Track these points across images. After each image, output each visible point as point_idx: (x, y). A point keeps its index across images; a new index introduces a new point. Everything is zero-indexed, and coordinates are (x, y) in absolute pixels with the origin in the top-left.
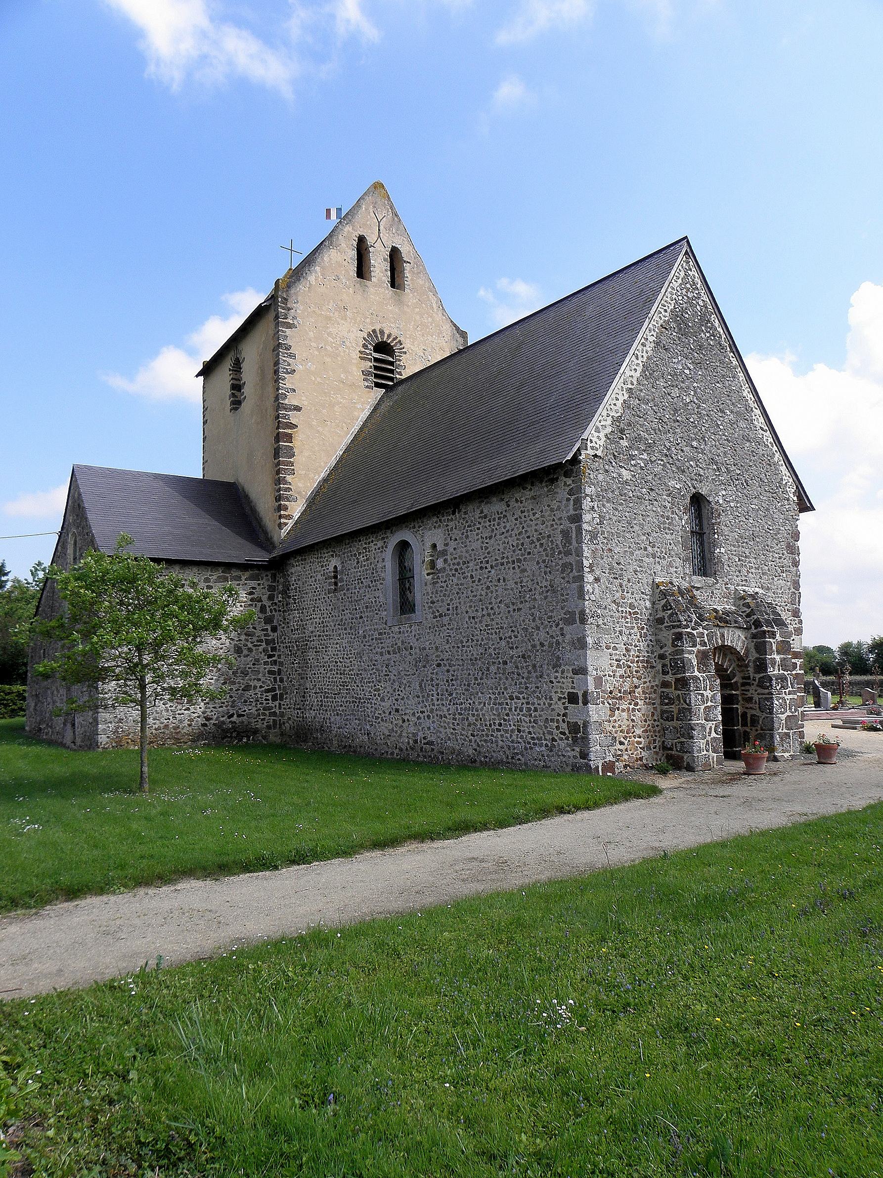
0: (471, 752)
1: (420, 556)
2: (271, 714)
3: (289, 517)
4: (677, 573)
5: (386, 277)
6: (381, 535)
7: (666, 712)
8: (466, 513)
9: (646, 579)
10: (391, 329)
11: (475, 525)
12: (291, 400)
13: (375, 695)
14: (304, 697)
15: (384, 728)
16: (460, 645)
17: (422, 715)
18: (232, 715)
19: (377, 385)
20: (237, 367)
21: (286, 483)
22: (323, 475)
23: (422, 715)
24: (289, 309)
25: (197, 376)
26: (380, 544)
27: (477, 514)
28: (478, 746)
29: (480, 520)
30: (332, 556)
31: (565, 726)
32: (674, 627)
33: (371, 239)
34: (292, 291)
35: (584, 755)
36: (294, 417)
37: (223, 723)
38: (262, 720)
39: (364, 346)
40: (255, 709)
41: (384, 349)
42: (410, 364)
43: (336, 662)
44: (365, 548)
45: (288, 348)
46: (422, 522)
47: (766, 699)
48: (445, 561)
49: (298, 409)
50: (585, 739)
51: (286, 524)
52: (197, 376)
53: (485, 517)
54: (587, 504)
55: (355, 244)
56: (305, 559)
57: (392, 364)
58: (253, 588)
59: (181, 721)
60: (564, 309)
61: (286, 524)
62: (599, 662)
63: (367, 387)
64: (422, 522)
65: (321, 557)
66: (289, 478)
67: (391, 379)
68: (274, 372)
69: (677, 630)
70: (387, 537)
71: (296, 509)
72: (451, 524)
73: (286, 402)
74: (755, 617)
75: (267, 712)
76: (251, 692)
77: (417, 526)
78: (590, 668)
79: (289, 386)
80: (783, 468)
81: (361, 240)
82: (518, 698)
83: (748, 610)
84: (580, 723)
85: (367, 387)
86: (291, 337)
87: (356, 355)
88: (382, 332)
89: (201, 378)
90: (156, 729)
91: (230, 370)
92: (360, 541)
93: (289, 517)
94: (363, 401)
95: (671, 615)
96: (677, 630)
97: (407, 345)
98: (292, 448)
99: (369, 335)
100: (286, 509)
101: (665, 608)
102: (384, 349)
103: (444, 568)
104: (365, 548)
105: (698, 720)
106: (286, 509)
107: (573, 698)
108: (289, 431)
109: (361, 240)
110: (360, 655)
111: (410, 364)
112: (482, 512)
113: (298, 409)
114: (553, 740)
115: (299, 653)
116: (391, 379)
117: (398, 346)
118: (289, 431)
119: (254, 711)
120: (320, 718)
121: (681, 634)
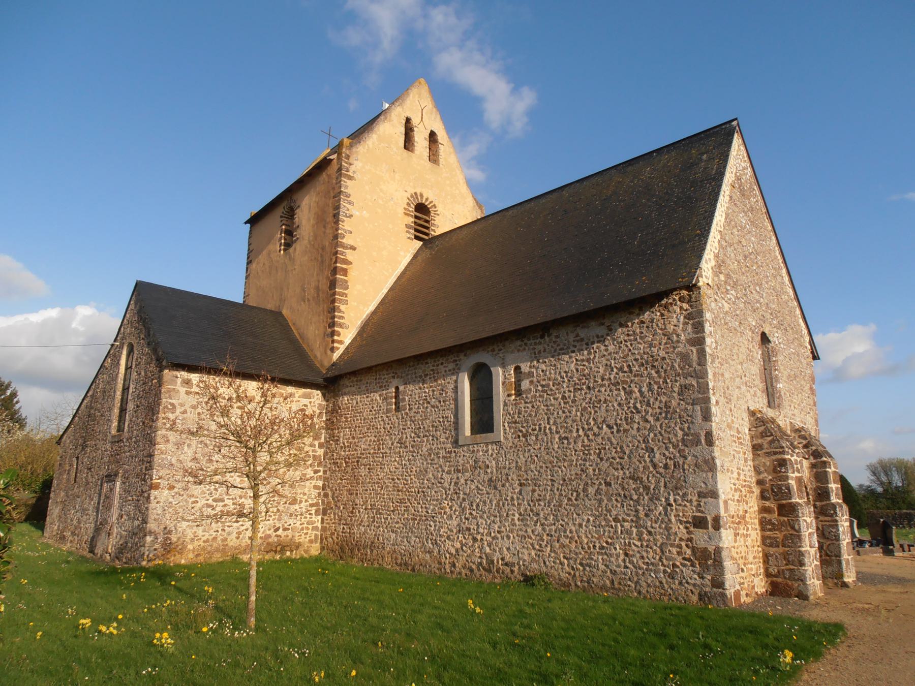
0: (564, 575)
1: (501, 376)
2: (313, 529)
3: (341, 342)
4: (759, 403)
5: (426, 153)
6: (452, 358)
7: (770, 538)
8: (557, 337)
9: (744, 407)
10: (430, 196)
11: (568, 348)
12: (347, 240)
13: (440, 513)
14: (352, 512)
15: (451, 547)
16: (550, 465)
17: (499, 535)
18: (278, 529)
19: (417, 238)
20: (291, 214)
21: (340, 311)
22: (372, 308)
23: (499, 535)
24: (351, 164)
25: (246, 223)
26: (451, 366)
27: (571, 338)
28: (573, 569)
29: (576, 343)
30: (393, 377)
31: (689, 552)
32: (775, 453)
33: (415, 121)
34: (354, 150)
35: (719, 584)
36: (349, 255)
37: (269, 536)
38: (306, 534)
39: (408, 204)
40: (299, 523)
41: (422, 209)
42: (442, 224)
43: (393, 479)
44: (433, 370)
45: (348, 196)
46: (504, 346)
47: (830, 526)
48: (531, 382)
49: (353, 248)
50: (718, 563)
51: (338, 349)
52: (246, 223)
53: (582, 340)
54: (708, 328)
55: (404, 122)
56: (361, 380)
57: (427, 222)
58: (305, 405)
59: (229, 534)
60: (565, 193)
61: (338, 349)
62: (725, 485)
63: (409, 238)
64: (504, 346)
65: (380, 379)
66: (343, 307)
67: (427, 234)
68: (332, 215)
69: (779, 457)
70: (460, 360)
71: (347, 336)
72: (540, 347)
73: (344, 241)
74: (814, 448)
75: (310, 527)
76: (297, 507)
77: (496, 349)
78: (721, 492)
79: (347, 227)
80: (801, 321)
81: (408, 120)
82: (624, 520)
83: (804, 442)
84: (711, 549)
85: (409, 238)
86: (349, 186)
87: (401, 211)
88: (421, 195)
89: (248, 225)
90: (204, 542)
91: (281, 217)
92: (427, 363)
93: (341, 342)
94: (406, 250)
95: (771, 442)
96: (779, 457)
97: (440, 209)
98: (346, 282)
99: (412, 196)
100: (339, 335)
101: (763, 435)
102: (422, 209)
103: (530, 389)
104: (433, 370)
105: (806, 548)
106: (339, 335)
107: (700, 523)
108: (344, 266)
109: (408, 120)
110: (423, 472)
111: (442, 224)
112: (577, 336)
113: (353, 248)
114: (674, 565)
115: (349, 469)
116: (427, 234)
117: (433, 209)
118: (344, 266)
119: (298, 525)
120: (371, 533)
121: (784, 460)
